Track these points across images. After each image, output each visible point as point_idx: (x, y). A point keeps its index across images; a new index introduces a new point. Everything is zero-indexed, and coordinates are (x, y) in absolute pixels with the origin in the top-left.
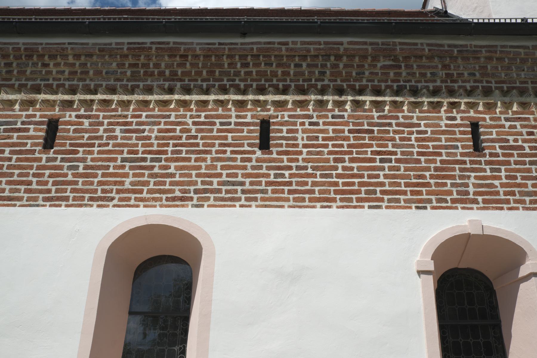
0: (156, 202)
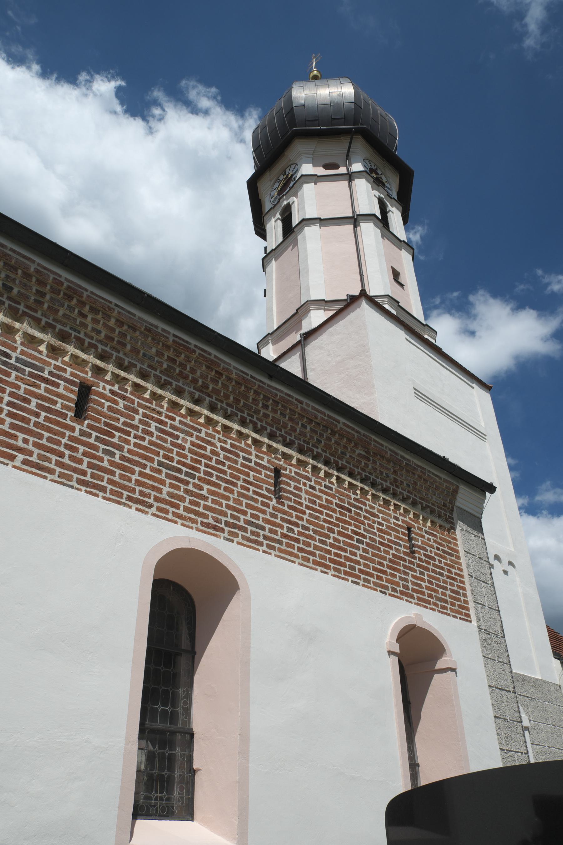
0: (192, 523)
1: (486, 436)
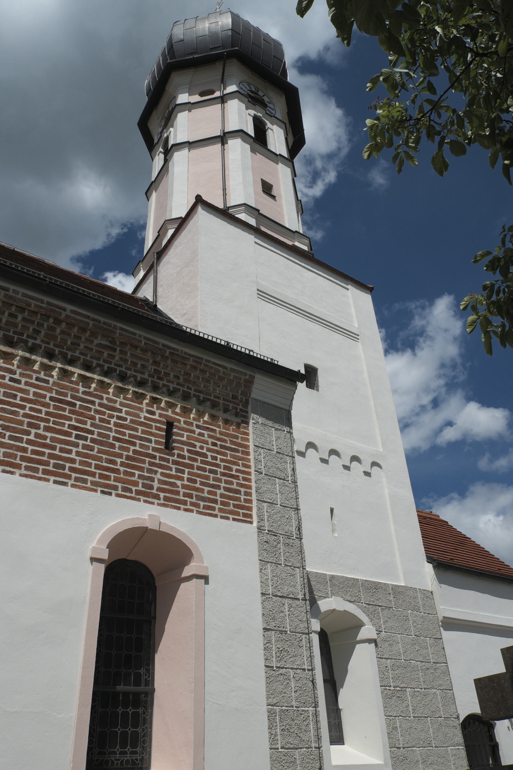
1: (358, 335)
